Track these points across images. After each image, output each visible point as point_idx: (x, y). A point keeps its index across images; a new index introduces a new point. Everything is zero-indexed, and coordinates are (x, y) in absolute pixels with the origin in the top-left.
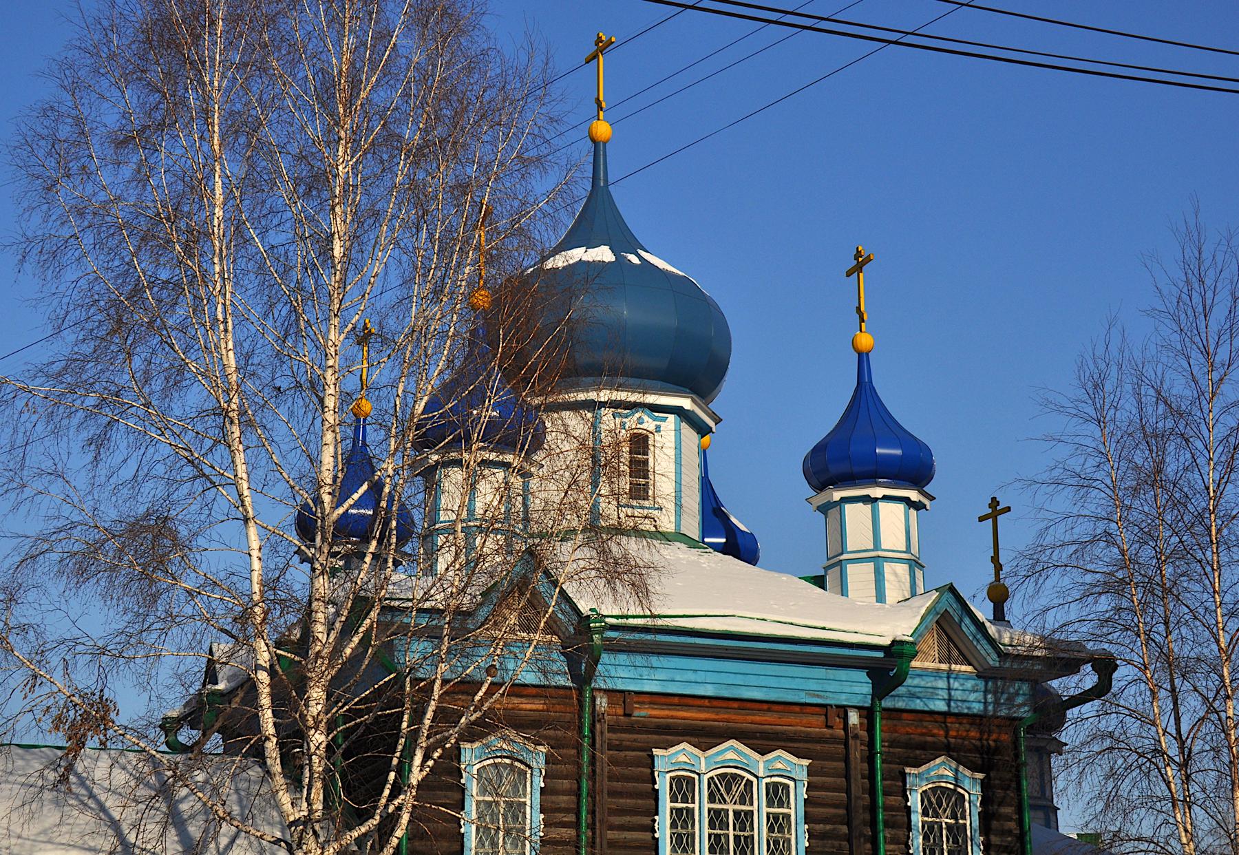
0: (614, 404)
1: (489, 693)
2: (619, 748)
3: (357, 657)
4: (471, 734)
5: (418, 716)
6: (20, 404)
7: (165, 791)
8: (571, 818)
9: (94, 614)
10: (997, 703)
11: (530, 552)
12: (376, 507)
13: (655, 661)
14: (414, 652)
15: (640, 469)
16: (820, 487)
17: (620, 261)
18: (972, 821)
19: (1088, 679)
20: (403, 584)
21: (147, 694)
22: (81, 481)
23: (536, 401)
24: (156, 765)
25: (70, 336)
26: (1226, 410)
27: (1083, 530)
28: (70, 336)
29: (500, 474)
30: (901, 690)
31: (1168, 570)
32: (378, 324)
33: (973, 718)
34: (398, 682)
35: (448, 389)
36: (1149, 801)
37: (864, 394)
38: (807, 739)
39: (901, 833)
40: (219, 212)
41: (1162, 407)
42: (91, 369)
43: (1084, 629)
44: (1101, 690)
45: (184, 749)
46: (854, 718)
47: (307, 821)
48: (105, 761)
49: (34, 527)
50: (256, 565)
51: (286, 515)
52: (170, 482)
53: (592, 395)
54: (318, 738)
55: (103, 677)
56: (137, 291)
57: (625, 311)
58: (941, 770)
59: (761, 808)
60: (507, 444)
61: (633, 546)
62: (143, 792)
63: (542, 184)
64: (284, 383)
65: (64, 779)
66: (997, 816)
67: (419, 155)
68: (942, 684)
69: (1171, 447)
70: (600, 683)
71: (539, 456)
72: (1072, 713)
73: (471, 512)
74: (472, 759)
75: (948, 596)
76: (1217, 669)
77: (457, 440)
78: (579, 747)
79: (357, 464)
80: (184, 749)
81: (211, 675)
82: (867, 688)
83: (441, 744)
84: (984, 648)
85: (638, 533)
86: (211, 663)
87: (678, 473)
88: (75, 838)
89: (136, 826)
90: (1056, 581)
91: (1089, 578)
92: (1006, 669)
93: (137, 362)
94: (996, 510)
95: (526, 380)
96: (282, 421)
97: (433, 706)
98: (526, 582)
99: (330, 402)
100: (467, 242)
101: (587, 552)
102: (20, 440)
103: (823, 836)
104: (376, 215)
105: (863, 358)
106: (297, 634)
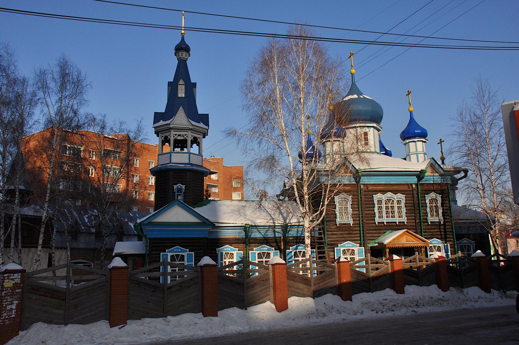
0: (360, 127)
1: (339, 186)
2: (366, 195)
3: (312, 181)
4: (336, 194)
5: (325, 191)
6: (245, 137)
7: (278, 208)
8: (358, 219)
9: (262, 175)
10: (444, 181)
11: (345, 157)
12: (314, 151)
13: (372, 177)
14: (323, 179)
15: (366, 139)
16: (404, 140)
17: (359, 98)
18: (439, 204)
19: (463, 174)
20: (320, 166)
21: (274, 189)
22: (257, 151)
23: (344, 127)
24: (276, 203)
25: (253, 123)
26: (489, 116)
27: (460, 144)
28: (253, 123)
29: (338, 142)
30: (423, 180)
31: (478, 151)
32: (312, 114)
33: (439, 184)
34: (321, 185)
35: (326, 126)
36: (476, 198)
37: (412, 120)
38: (404, 191)
39: (425, 208)
40: (278, 96)
41: (475, 117)
42: (257, 129)
43: (461, 164)
44: (465, 176)
45: (281, 200)
46: (414, 186)
47: (306, 213)
48: (267, 203)
49: (250, 160)
50: (291, 164)
51: (297, 154)
52: (274, 149)
53: (355, 125)
54: (306, 197)
55: (265, 187)
56: (264, 113)
57: (361, 107)
58: (433, 195)
59: (396, 205)
60: (339, 136)
61: (366, 155)
62: (274, 208)
63: (342, 83)
64: (294, 128)
65: (260, 207)
66: (445, 203)
67: (317, 80)
68: (432, 178)
69: (478, 125)
70: (361, 183)
71: (345, 138)
72: (459, 182)
73: (333, 151)
74: (337, 199)
75: (432, 160)
76: (489, 170)
77: (329, 136)
78: (358, 195)
79: (309, 143)
80: (281, 200)
81: (285, 186)
82: (416, 180)
83: (330, 196)
84: (440, 170)
85: (367, 152)
86: (284, 183)
87: (374, 139)
88: (263, 217)
89: (274, 215)
90: (455, 155)
91: (462, 154)
92: (445, 174)
93: (265, 126)
94: (441, 142)
95: (342, 123)
96: (294, 135)
97: (328, 189)
98: (345, 164)
99: (303, 131)
100: (328, 96)
101: (356, 157)
102: (245, 144)
103: (409, 210)
104: (309, 93)
105: (411, 113)
106: (300, 177)
